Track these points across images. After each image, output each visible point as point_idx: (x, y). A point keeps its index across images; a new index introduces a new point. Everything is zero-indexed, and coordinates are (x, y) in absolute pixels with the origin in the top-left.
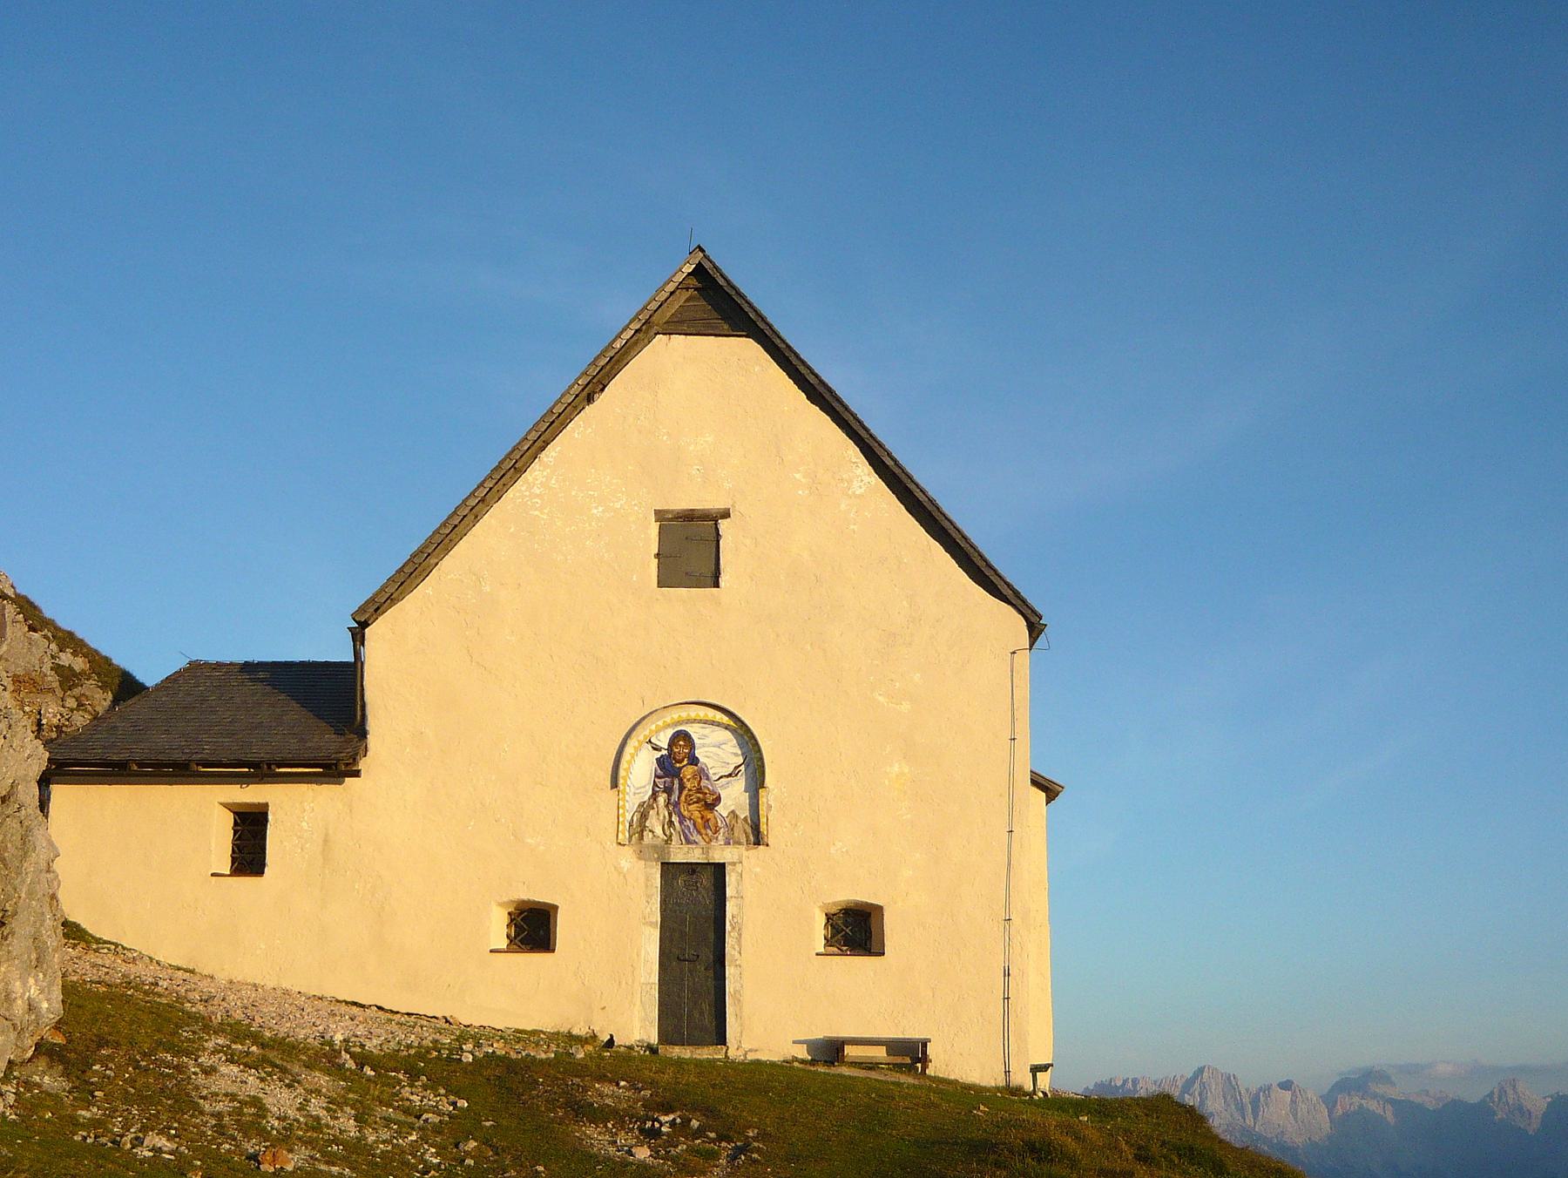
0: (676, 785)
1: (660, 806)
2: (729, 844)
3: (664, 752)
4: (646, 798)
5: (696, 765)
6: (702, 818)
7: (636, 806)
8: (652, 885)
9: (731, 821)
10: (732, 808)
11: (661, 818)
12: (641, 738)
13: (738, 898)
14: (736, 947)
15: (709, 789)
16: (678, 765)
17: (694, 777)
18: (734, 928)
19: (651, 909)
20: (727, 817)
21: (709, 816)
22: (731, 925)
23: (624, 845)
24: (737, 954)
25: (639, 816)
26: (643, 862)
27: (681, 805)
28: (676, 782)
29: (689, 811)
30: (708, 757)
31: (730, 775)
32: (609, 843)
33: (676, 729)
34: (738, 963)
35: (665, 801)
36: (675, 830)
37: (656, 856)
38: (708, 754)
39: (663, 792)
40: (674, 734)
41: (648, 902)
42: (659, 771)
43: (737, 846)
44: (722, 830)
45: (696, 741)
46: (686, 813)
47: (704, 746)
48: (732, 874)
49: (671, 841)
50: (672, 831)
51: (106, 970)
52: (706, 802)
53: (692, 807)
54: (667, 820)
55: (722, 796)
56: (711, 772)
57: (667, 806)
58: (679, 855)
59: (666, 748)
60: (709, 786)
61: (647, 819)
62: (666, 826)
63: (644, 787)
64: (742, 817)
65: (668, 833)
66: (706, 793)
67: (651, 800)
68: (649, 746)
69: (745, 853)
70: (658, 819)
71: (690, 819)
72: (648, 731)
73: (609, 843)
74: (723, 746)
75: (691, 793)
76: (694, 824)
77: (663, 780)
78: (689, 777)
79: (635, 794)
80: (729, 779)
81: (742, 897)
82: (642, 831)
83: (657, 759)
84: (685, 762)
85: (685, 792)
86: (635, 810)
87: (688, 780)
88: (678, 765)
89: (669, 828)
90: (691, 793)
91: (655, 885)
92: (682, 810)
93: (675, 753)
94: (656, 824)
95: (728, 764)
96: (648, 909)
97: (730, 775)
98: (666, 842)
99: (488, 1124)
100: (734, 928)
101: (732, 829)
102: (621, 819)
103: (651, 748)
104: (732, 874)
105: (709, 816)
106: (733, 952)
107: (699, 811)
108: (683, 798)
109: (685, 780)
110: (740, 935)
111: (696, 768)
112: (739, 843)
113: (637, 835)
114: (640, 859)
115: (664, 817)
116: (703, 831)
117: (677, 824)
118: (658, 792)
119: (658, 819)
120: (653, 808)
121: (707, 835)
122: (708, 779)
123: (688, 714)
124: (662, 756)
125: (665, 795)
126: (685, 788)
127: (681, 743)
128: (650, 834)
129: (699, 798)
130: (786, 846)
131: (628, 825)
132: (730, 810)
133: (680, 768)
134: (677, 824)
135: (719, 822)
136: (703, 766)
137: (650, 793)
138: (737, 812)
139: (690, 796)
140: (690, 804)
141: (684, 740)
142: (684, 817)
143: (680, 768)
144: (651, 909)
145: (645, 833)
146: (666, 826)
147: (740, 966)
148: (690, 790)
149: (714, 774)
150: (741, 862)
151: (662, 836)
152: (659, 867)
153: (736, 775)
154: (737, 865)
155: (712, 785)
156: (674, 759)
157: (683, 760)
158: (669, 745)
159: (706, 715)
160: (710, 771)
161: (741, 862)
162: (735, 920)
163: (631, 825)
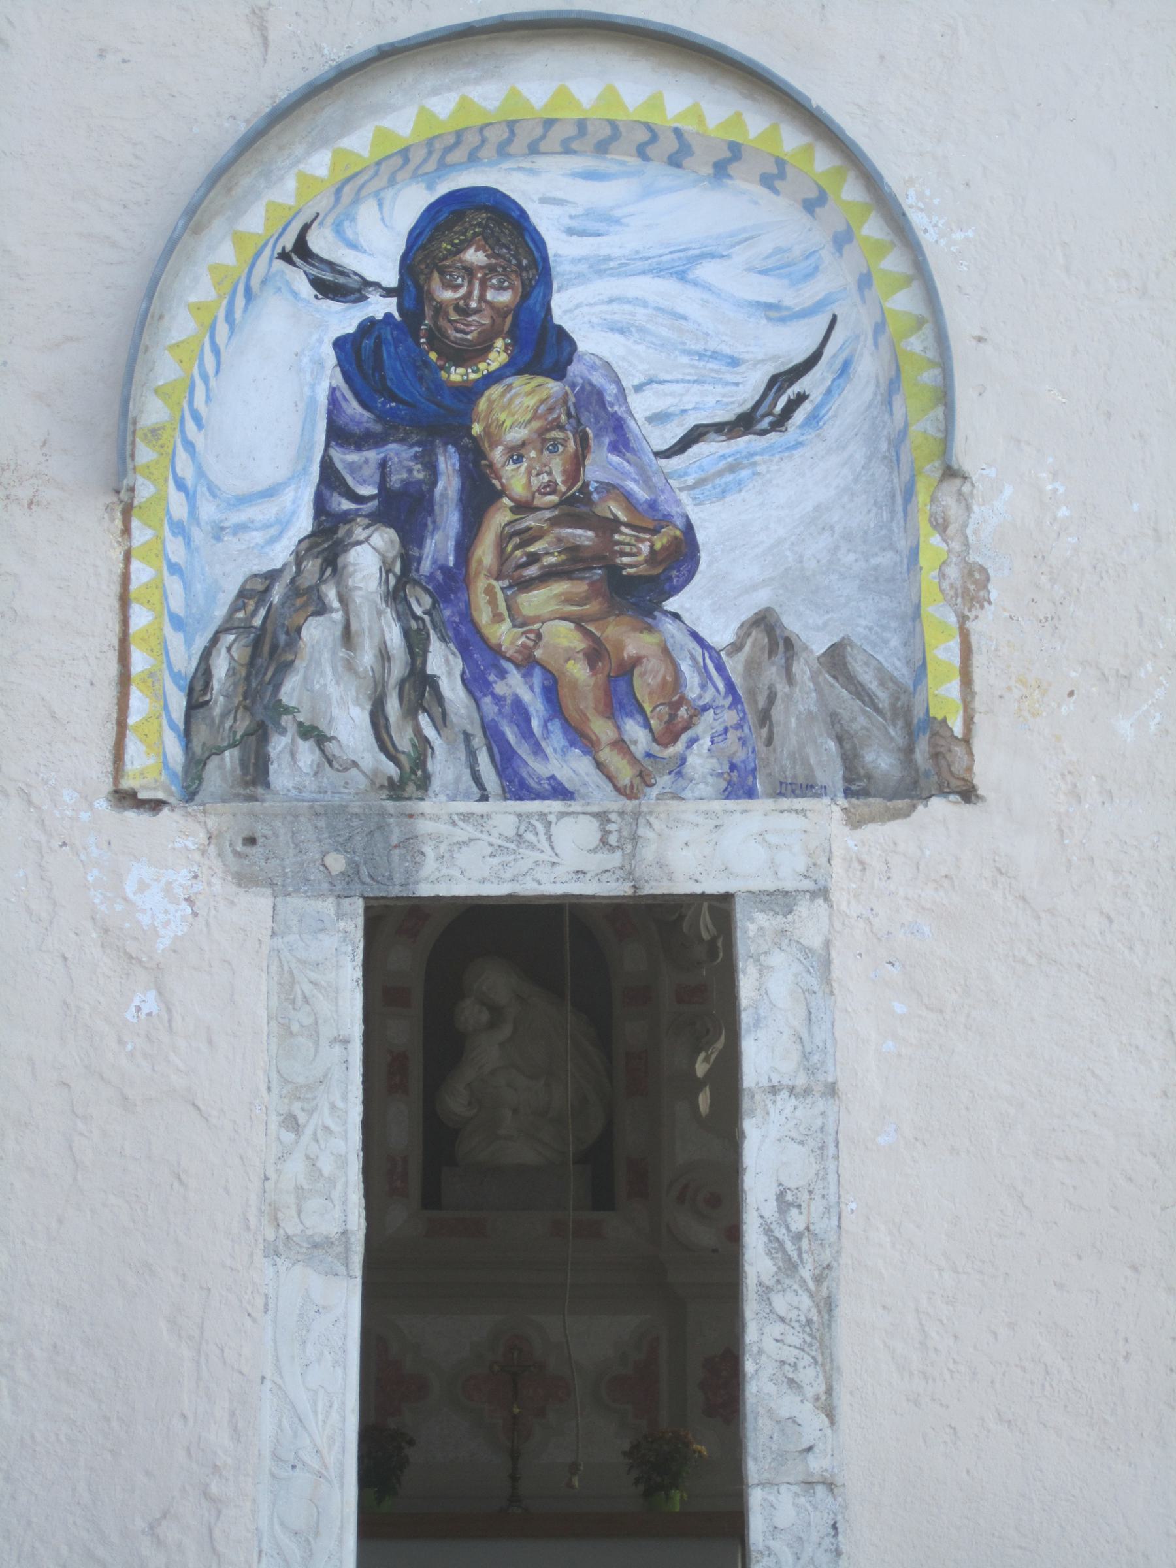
0: (449, 484)
1: (358, 598)
2: (751, 794)
3: (380, 307)
4: (280, 554)
5: (558, 373)
6: (595, 654)
7: (231, 589)
8: (314, 1033)
9: (752, 668)
10: (760, 599)
11: (367, 658)
12: (255, 222)
13: (808, 1091)
14: (809, 1376)
15: (627, 499)
16: (456, 375)
17: (544, 441)
18: (790, 1267)
19: (312, 1162)
20: (735, 648)
21: (635, 643)
22: (775, 1246)
23: (156, 806)
24: (813, 1423)
25: (241, 653)
26: (261, 902)
27: (481, 584)
28: (448, 463)
29: (518, 621)
30: (622, 330)
31: (744, 424)
32: (68, 796)
33: (443, 189)
34: (816, 1464)
35: (386, 568)
36: (442, 721)
37: (337, 863)
38: (620, 313)
39: (379, 518)
40: (433, 210)
41: (291, 1122)
42: (353, 407)
43: (799, 803)
44: (706, 726)
45: (558, 245)
46: (503, 634)
47: (600, 267)
48: (777, 959)
49: (424, 783)
50: (429, 732)
51: (212, 909)
52: (613, 571)
53: (535, 601)
54: (398, 669)
55: (701, 537)
56: (641, 406)
57: (396, 596)
58: (464, 857)
59: (391, 279)
60: (631, 486)
61: (286, 667)
62: (393, 707)
63: (270, 493)
64: (819, 645)
65: (403, 741)
66: (614, 524)
67: (312, 566)
68: (298, 279)
69: (846, 841)
70: (350, 666)
71: (527, 663)
72: (291, 184)
73: (68, 796)
74: (707, 271)
75: (530, 521)
76: (552, 692)
77: (373, 455)
78: (516, 435)
79: (218, 532)
80: (744, 443)
81: (832, 1090)
82: (260, 734)
83: (340, 344)
84: (497, 358)
85: (499, 518)
86: (220, 613)
87: (516, 453)
88: (456, 375)
89: (411, 711)
90: (530, 521)
91: (327, 1032)
92: (483, 617)
93: (440, 309)
94: (334, 691)
95: (734, 362)
96: (296, 1168)
97: (744, 424)
98: (395, 789)
99: (1044, 475)
100: (790, 1267)
101: (765, 718)
102: (139, 661)
103: (306, 290)
104: (777, 959)
105: (635, 643)
106: (789, 1405)
107: (579, 622)
108: (485, 552)
109: (497, 455)
110: (828, 1305)
111: (553, 387)
112: (807, 788)
113: (230, 757)
114: (244, 880)
115: (384, 655)
116: (601, 729)
117: (453, 691)
118: (346, 518)
119: (350, 666)
120: (322, 609)
121: (621, 745)
122: (622, 441)
123: (514, 94)
124: (368, 327)
125: (384, 539)
126: (497, 495)
127: (474, 256)
128: (307, 754)
129: (573, 551)
130: (1076, 795)
131: (178, 702)
132: (747, 614)
133: (470, 393)
134: (453, 691)
135: (692, 679)
136: (598, 379)
137: (304, 523)
138: (792, 624)
139: (528, 537)
140: (526, 585)
141: (490, 242)
142: (496, 652)
143: (470, 393)
144: (312, 1162)
145: (278, 745)
146: (393, 707)
147: (830, 1486)
148: (523, 507)
149: (659, 418)
150: (822, 893)
151: (369, 757)
152: (355, 927)
153: (780, 422)
154: (803, 908)
155: (645, 480)
156: (437, 339)
157: (482, 349)
158: (408, 265)
159: (610, 95)
160: (634, 400)
161: (822, 893)
162: (797, 1221)
163: (196, 703)
